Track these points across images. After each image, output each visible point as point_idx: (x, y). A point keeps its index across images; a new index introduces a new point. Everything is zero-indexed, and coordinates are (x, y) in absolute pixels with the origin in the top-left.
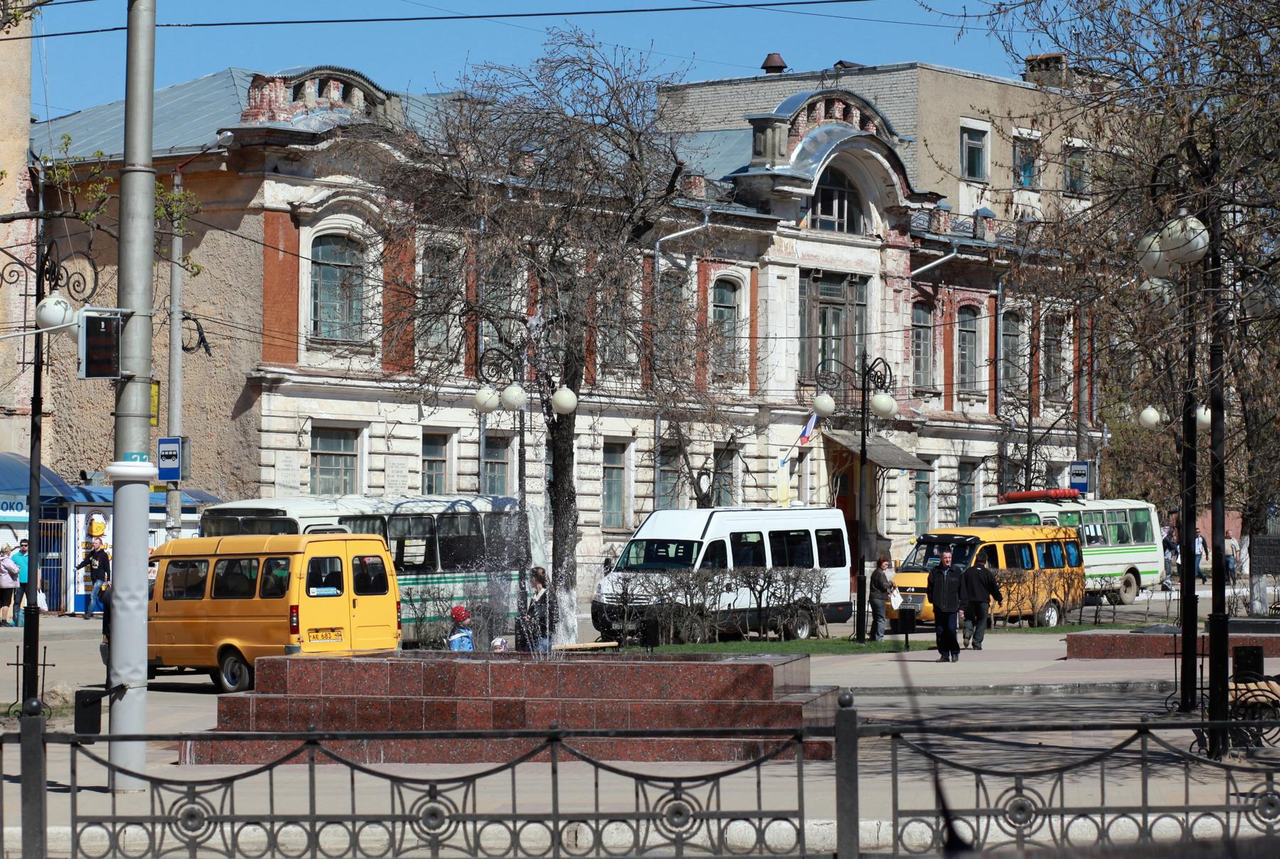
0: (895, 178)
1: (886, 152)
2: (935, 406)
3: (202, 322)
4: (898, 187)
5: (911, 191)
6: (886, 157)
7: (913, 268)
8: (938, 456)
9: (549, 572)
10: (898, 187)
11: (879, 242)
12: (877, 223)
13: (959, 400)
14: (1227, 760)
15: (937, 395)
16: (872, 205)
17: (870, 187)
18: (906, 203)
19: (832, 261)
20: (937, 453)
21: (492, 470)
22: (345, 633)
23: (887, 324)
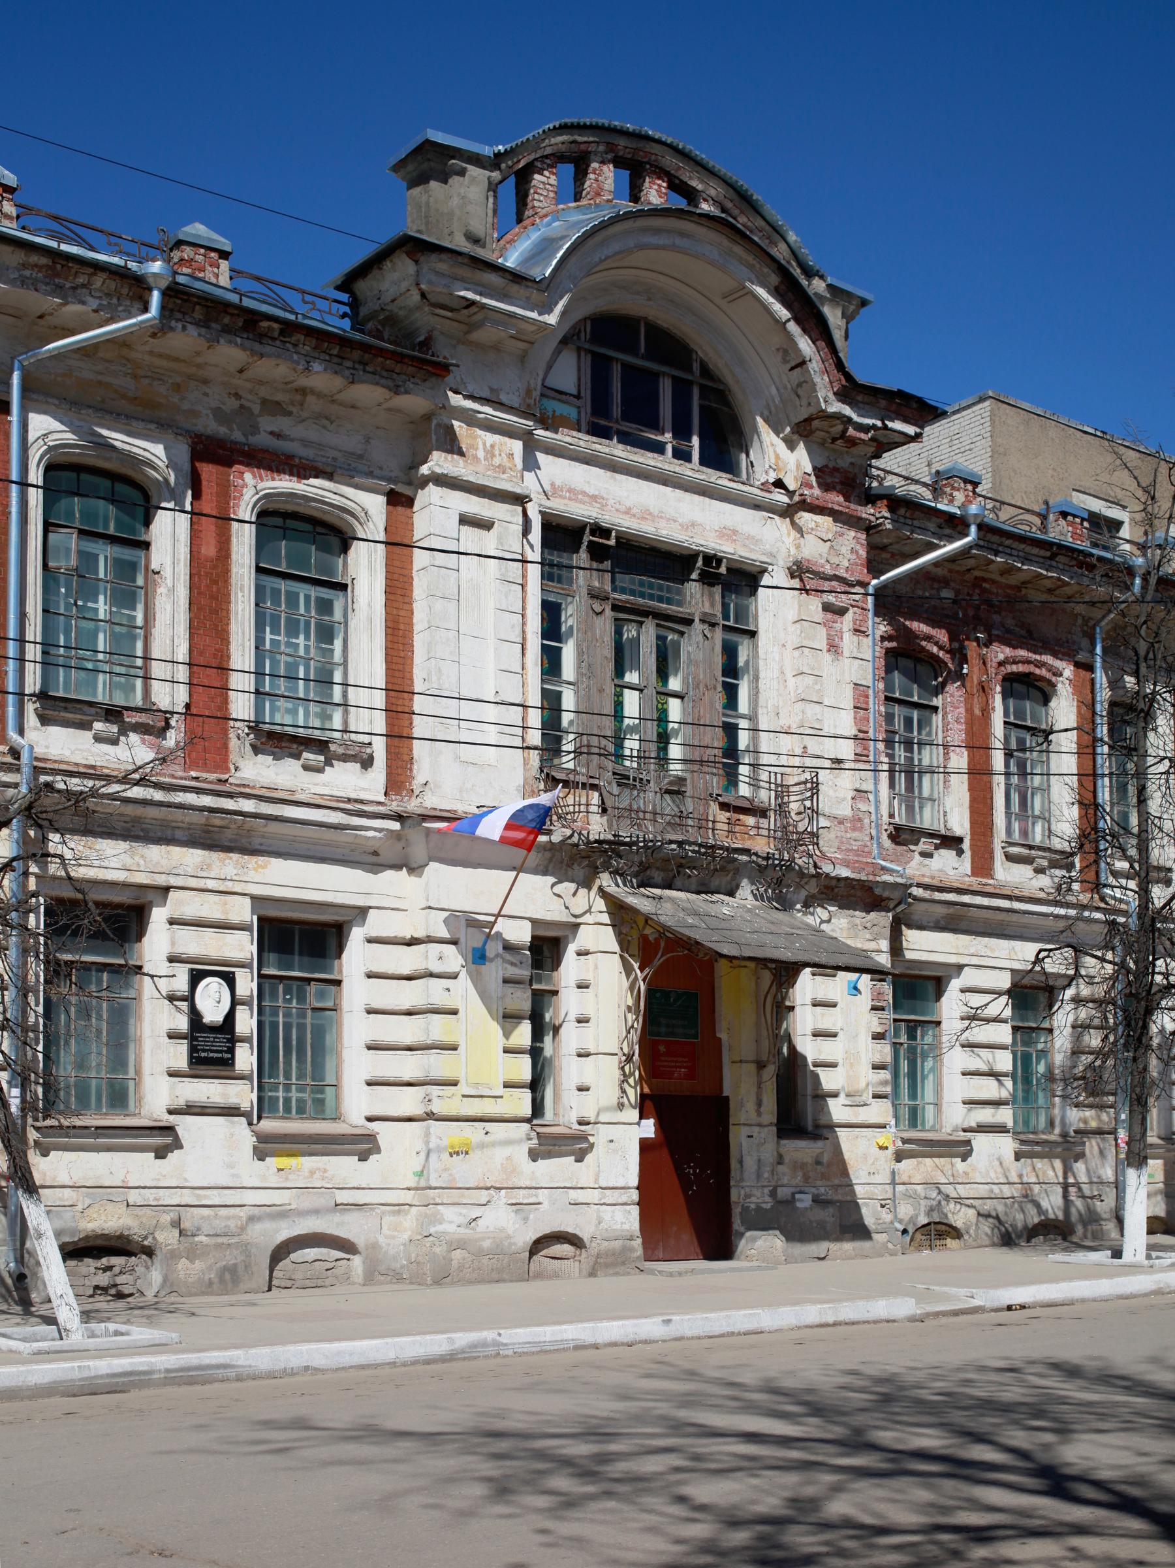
0: (805, 345)
1: (774, 279)
2: (949, 867)
3: (605, 793)
4: (815, 366)
5: (848, 377)
6: (778, 293)
7: (875, 566)
8: (960, 968)
9: (1023, 953)
10: (815, 366)
11: (781, 498)
12: (779, 458)
13: (1010, 858)
14: (1167, 763)
15: (951, 842)
16: (759, 420)
17: (753, 378)
18: (836, 407)
19: (646, 515)
20: (952, 959)
21: (912, 1036)
22: (461, 1049)
23: (808, 679)
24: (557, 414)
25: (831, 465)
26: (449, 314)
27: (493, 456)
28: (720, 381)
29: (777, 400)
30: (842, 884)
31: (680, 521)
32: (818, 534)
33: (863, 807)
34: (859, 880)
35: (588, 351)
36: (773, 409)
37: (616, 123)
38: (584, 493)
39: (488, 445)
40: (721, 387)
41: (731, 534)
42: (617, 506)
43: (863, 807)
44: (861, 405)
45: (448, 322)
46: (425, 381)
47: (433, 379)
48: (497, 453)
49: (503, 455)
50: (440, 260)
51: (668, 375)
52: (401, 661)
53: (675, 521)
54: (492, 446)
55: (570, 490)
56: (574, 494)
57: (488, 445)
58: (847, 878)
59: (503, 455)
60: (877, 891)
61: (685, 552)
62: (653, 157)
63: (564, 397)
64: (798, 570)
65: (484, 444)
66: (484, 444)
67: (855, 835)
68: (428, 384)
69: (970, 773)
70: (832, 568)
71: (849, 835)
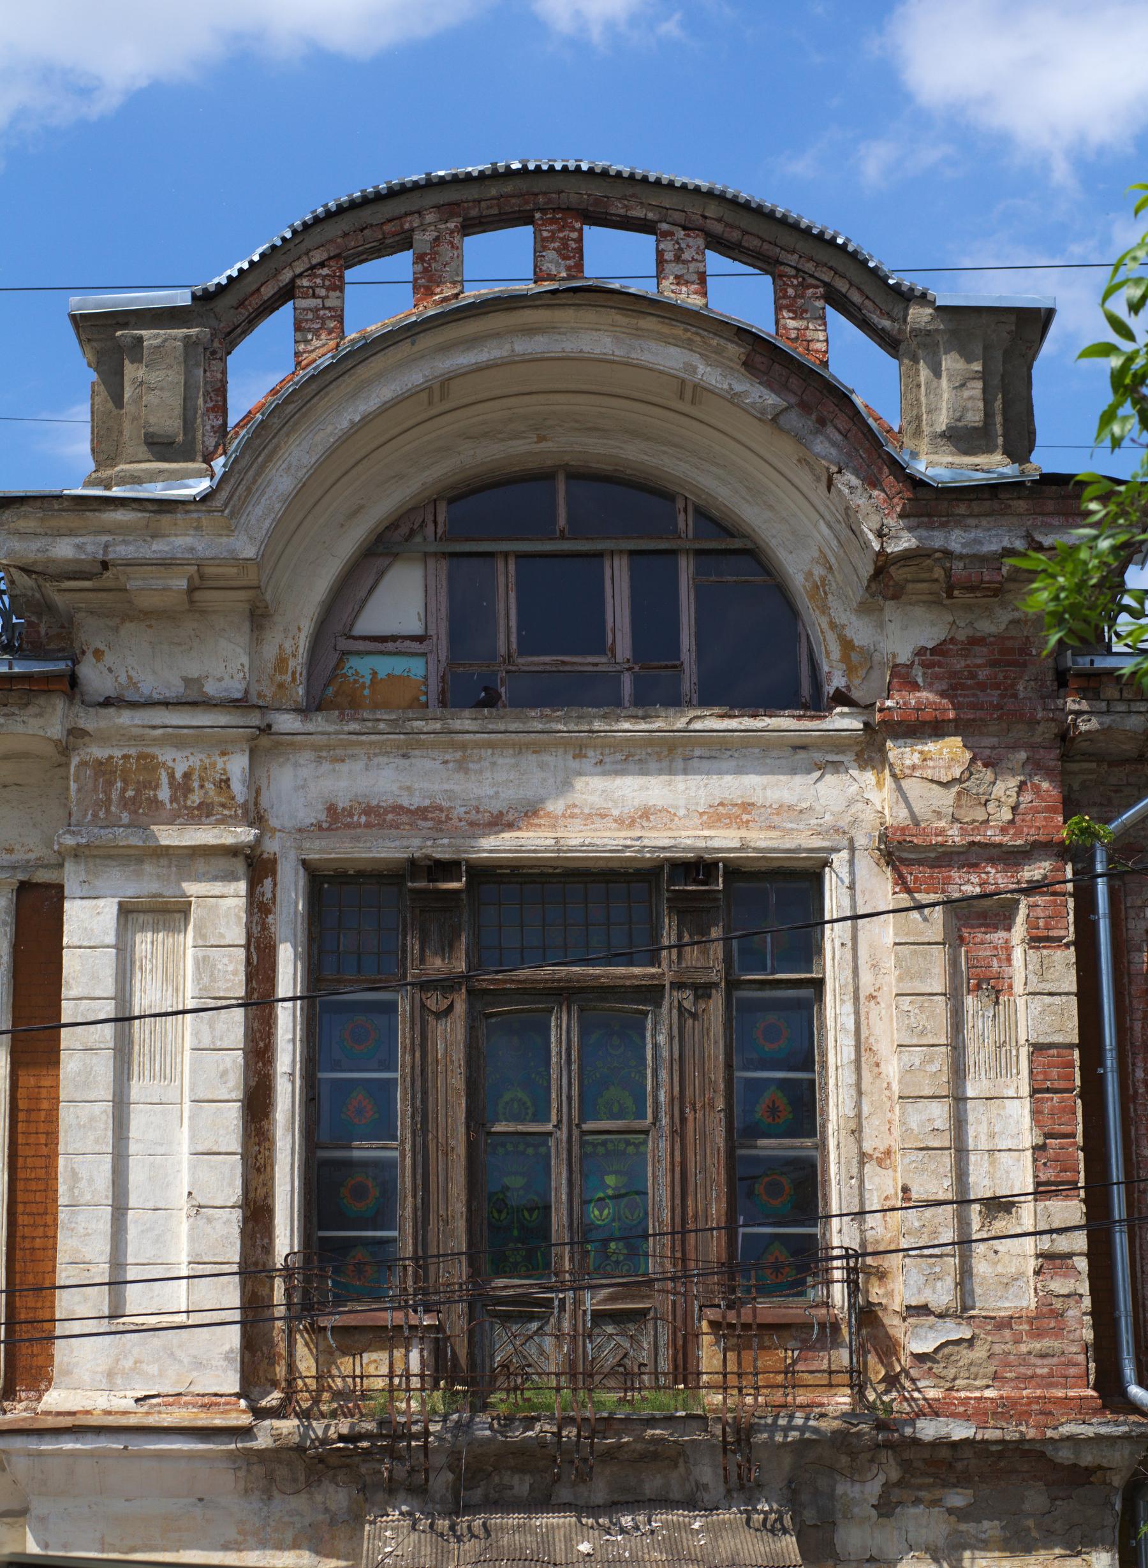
24: (382, 675)
25: (961, 636)
26: (87, 584)
27: (188, 790)
28: (744, 536)
29: (834, 544)
30: (968, 1453)
31: (616, 812)
32: (929, 774)
33: (1060, 1286)
34: (1002, 1441)
35: (436, 555)
36: (833, 560)
37: (441, 173)
38: (399, 809)
39: (178, 776)
40: (750, 546)
41: (742, 811)
42: (473, 816)
43: (1060, 1286)
44: (972, 522)
45: (91, 595)
46: (27, 705)
47: (42, 701)
48: (196, 785)
49: (209, 786)
50: (25, 516)
51: (621, 552)
52: (41, 1162)
53: (603, 816)
54: (187, 776)
55: (368, 811)
56: (378, 816)
57: (178, 776)
58: (966, 1442)
59: (209, 786)
60: (1065, 1455)
61: (648, 865)
62: (541, 199)
63: (390, 646)
64: (900, 853)
65: (172, 776)
66: (172, 776)
67: (1045, 1344)
68: (32, 710)
69: (242, 1323)
70: (963, 832)
71: (1024, 1348)
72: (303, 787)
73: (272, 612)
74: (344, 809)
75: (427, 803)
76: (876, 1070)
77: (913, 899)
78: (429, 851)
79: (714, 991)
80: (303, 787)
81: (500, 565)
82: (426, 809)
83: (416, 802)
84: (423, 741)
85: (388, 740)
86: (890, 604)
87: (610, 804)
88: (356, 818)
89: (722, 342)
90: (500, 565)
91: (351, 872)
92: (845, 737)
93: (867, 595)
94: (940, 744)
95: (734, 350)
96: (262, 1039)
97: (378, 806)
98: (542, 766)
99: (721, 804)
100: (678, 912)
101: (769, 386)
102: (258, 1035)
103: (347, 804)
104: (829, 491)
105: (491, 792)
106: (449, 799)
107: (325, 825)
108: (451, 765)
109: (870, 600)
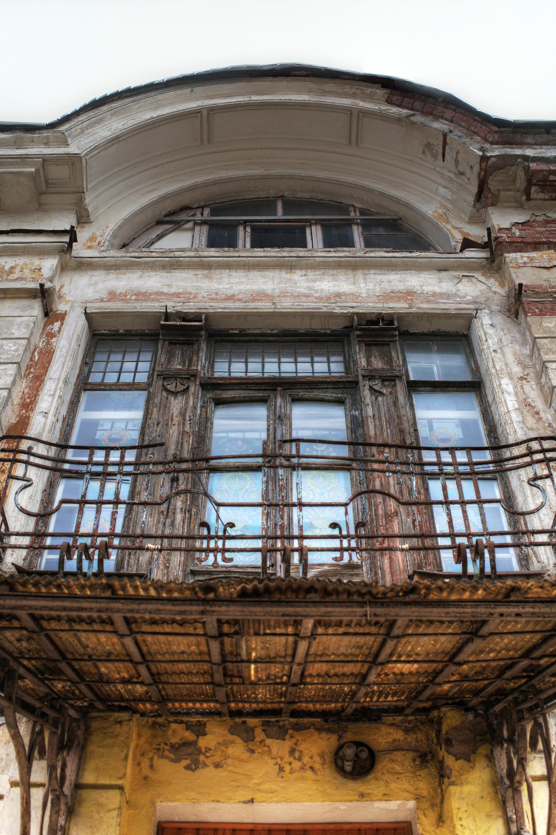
55: (138, 294)
72: (94, 285)
73: (92, 220)
74: (121, 293)
75: (181, 291)
76: (537, 416)
77: (541, 445)
78: (179, 309)
79: (398, 382)
80: (94, 285)
81: (241, 229)
82: (180, 293)
83: (173, 290)
84: (182, 261)
85: (157, 261)
86: (490, 210)
87: (312, 292)
88: (128, 297)
89: (373, 90)
90: (241, 229)
91: (121, 331)
92: (473, 262)
93: (474, 210)
94: (540, 253)
95: (381, 92)
96: (29, 398)
97: (146, 292)
98: (264, 277)
99: (392, 292)
100: (366, 345)
101: (396, 800)
102: (27, 395)
103: (123, 291)
104: (444, 160)
105: (228, 286)
106: (197, 290)
107: (105, 300)
108: (199, 276)
109: (476, 214)
